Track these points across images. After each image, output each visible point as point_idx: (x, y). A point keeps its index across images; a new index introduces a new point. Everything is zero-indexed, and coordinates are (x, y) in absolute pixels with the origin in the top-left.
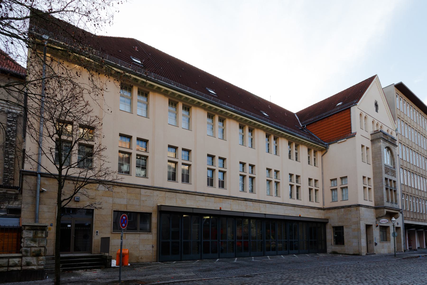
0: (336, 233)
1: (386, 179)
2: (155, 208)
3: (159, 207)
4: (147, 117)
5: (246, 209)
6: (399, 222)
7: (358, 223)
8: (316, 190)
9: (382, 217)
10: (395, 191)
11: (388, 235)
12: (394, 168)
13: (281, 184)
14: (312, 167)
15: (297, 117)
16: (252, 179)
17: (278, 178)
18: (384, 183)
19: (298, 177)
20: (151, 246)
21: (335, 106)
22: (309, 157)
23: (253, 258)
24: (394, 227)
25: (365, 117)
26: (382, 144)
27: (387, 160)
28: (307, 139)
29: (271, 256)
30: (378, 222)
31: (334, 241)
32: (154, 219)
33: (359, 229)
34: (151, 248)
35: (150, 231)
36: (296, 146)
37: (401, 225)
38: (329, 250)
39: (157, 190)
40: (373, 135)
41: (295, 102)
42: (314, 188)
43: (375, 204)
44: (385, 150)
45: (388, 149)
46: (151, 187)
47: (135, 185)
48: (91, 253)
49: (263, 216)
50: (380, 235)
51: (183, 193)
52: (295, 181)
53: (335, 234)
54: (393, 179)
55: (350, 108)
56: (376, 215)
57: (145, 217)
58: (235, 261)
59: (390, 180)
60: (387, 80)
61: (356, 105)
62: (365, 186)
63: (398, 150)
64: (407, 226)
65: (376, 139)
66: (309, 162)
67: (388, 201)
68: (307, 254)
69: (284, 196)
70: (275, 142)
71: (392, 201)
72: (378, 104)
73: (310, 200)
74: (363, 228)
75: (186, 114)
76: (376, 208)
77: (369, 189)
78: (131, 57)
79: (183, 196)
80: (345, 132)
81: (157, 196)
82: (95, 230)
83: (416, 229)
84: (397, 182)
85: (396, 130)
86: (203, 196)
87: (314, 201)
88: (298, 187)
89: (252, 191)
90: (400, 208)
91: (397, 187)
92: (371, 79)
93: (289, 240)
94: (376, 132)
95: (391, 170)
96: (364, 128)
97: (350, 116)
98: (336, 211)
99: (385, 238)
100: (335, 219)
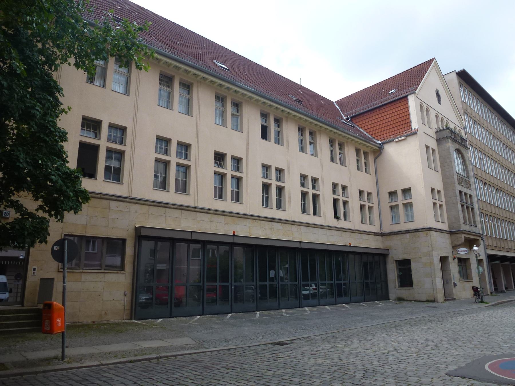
0: (400, 270)
1: (460, 192)
2: (132, 232)
3: (138, 230)
4: (127, 92)
7: (429, 255)
8: (370, 208)
9: (460, 246)
11: (468, 271)
12: (468, 177)
15: (337, 107)
19: (344, 188)
20: (123, 293)
21: (386, 94)
22: (358, 160)
23: (284, 310)
26: (450, 146)
27: (458, 167)
30: (455, 253)
31: (398, 282)
33: (432, 264)
34: (122, 297)
35: (121, 268)
37: (483, 257)
38: (392, 295)
39: (137, 203)
40: (438, 133)
43: (449, 227)
44: (455, 155)
45: (458, 151)
46: (127, 198)
47: (101, 194)
48: (23, 306)
49: (298, 246)
50: (460, 272)
51: (176, 209)
52: (341, 194)
53: (400, 272)
54: (469, 192)
55: (406, 97)
56: (452, 242)
57: (115, 245)
60: (449, 65)
62: (435, 201)
63: (471, 154)
64: (491, 258)
65: (443, 138)
66: (358, 167)
67: (465, 223)
68: (361, 302)
69: (252, 201)
71: (470, 222)
72: (440, 93)
74: (437, 262)
75: (185, 93)
76: (451, 233)
77: (441, 206)
78: (215, 61)
79: (177, 213)
80: (402, 128)
81: (136, 212)
82: (31, 266)
83: (501, 262)
84: (473, 197)
86: (207, 213)
88: (345, 203)
89: (280, 205)
90: (481, 233)
92: (428, 63)
93: (336, 282)
96: (426, 124)
99: (465, 275)
100: (398, 250)
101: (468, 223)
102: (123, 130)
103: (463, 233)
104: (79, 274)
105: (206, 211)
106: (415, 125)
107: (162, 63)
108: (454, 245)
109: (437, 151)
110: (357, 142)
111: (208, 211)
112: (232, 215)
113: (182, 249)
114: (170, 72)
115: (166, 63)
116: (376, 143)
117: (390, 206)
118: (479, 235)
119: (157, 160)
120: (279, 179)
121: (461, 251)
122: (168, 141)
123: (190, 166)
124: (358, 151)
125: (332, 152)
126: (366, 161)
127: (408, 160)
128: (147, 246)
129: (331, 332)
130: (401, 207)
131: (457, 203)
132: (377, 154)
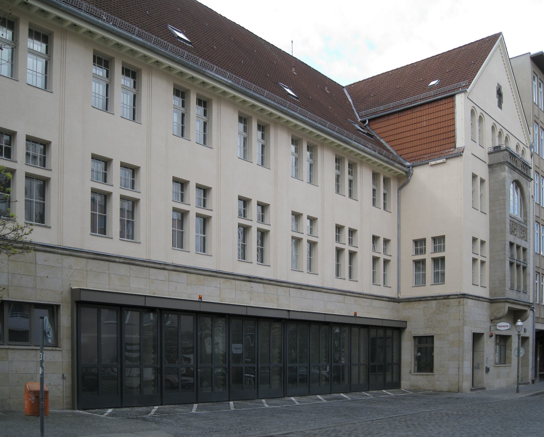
0: (419, 350)
1: (511, 244)
2: (67, 295)
5: (251, 299)
6: (528, 327)
8: (386, 262)
9: (500, 319)
10: (524, 268)
11: (508, 352)
12: (525, 222)
13: (271, 235)
14: (379, 212)
15: (348, 97)
16: (205, 220)
17: (208, 205)
18: (508, 253)
19: (352, 232)
22: (374, 190)
23: (263, 401)
24: (519, 338)
25: (480, 117)
26: (507, 175)
28: (373, 152)
29: (268, 400)
32: (65, 319)
34: (61, 381)
36: (351, 166)
37: (530, 334)
38: (405, 383)
39: (70, 255)
40: (492, 156)
41: (345, 72)
42: (347, 248)
44: (511, 188)
45: (518, 184)
46: (58, 248)
51: (123, 263)
52: (382, 250)
54: (523, 244)
55: (453, 96)
58: (194, 411)
59: (518, 247)
61: (465, 91)
62: (475, 256)
65: (498, 164)
66: (374, 200)
67: (512, 288)
69: (223, 252)
70: (260, 133)
71: (519, 287)
72: (503, 91)
73: (338, 274)
74: (468, 340)
77: (483, 263)
78: (170, 27)
79: (124, 269)
84: (528, 251)
85: (531, 147)
86: (164, 269)
87: (382, 283)
88: (352, 254)
89: (203, 247)
90: (531, 301)
91: (528, 261)
94: (497, 149)
95: (519, 227)
96: (477, 141)
97: (454, 113)
98: (422, 305)
100: (418, 323)
101: (516, 288)
102: (46, 145)
103: (507, 302)
104: (5, 351)
105: (162, 266)
106: (460, 143)
107: (96, 38)
108: (493, 318)
109: (487, 183)
110: (375, 163)
111: (166, 267)
112: (198, 272)
113: (130, 317)
114: (107, 52)
115: (104, 38)
116: (402, 165)
117: (414, 261)
118: (529, 305)
119: (94, 191)
120: (262, 219)
121: (501, 326)
122: (107, 162)
123: (139, 200)
124: (375, 176)
125: (338, 177)
126: (386, 192)
127: (447, 194)
128: (89, 315)
129: (329, 426)
130: (429, 264)
131: (505, 260)
132: (402, 183)
